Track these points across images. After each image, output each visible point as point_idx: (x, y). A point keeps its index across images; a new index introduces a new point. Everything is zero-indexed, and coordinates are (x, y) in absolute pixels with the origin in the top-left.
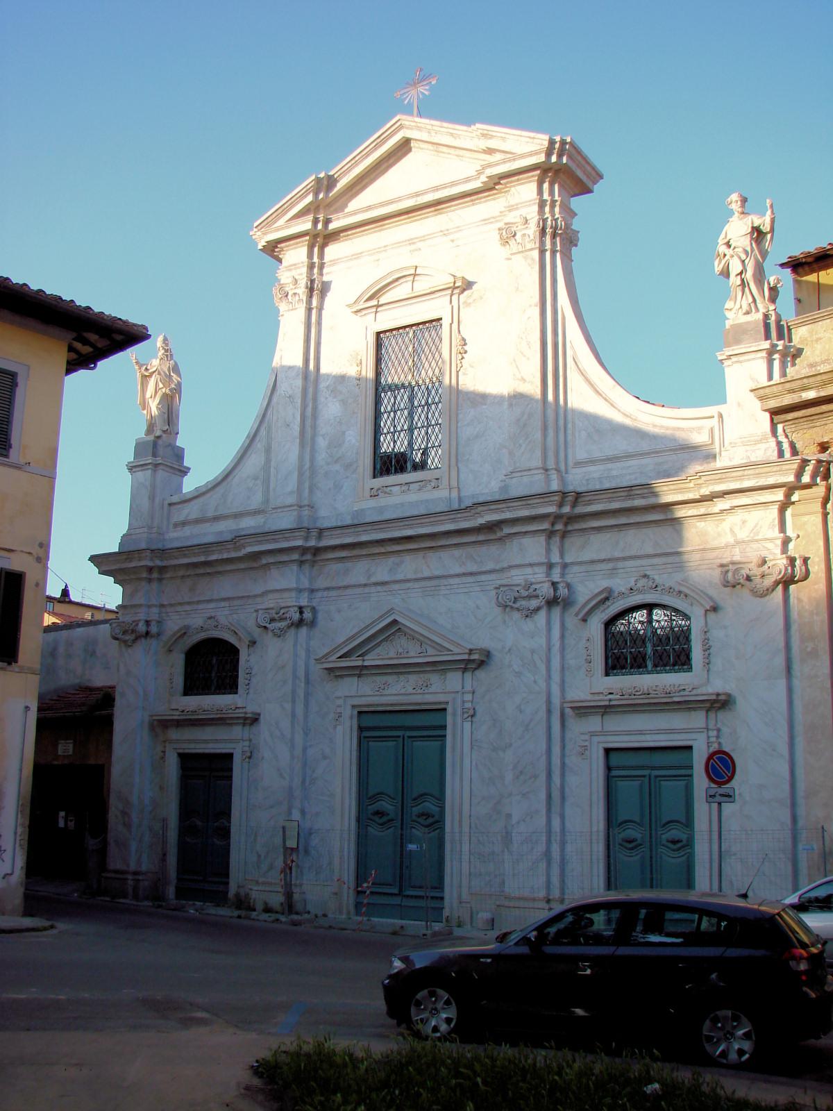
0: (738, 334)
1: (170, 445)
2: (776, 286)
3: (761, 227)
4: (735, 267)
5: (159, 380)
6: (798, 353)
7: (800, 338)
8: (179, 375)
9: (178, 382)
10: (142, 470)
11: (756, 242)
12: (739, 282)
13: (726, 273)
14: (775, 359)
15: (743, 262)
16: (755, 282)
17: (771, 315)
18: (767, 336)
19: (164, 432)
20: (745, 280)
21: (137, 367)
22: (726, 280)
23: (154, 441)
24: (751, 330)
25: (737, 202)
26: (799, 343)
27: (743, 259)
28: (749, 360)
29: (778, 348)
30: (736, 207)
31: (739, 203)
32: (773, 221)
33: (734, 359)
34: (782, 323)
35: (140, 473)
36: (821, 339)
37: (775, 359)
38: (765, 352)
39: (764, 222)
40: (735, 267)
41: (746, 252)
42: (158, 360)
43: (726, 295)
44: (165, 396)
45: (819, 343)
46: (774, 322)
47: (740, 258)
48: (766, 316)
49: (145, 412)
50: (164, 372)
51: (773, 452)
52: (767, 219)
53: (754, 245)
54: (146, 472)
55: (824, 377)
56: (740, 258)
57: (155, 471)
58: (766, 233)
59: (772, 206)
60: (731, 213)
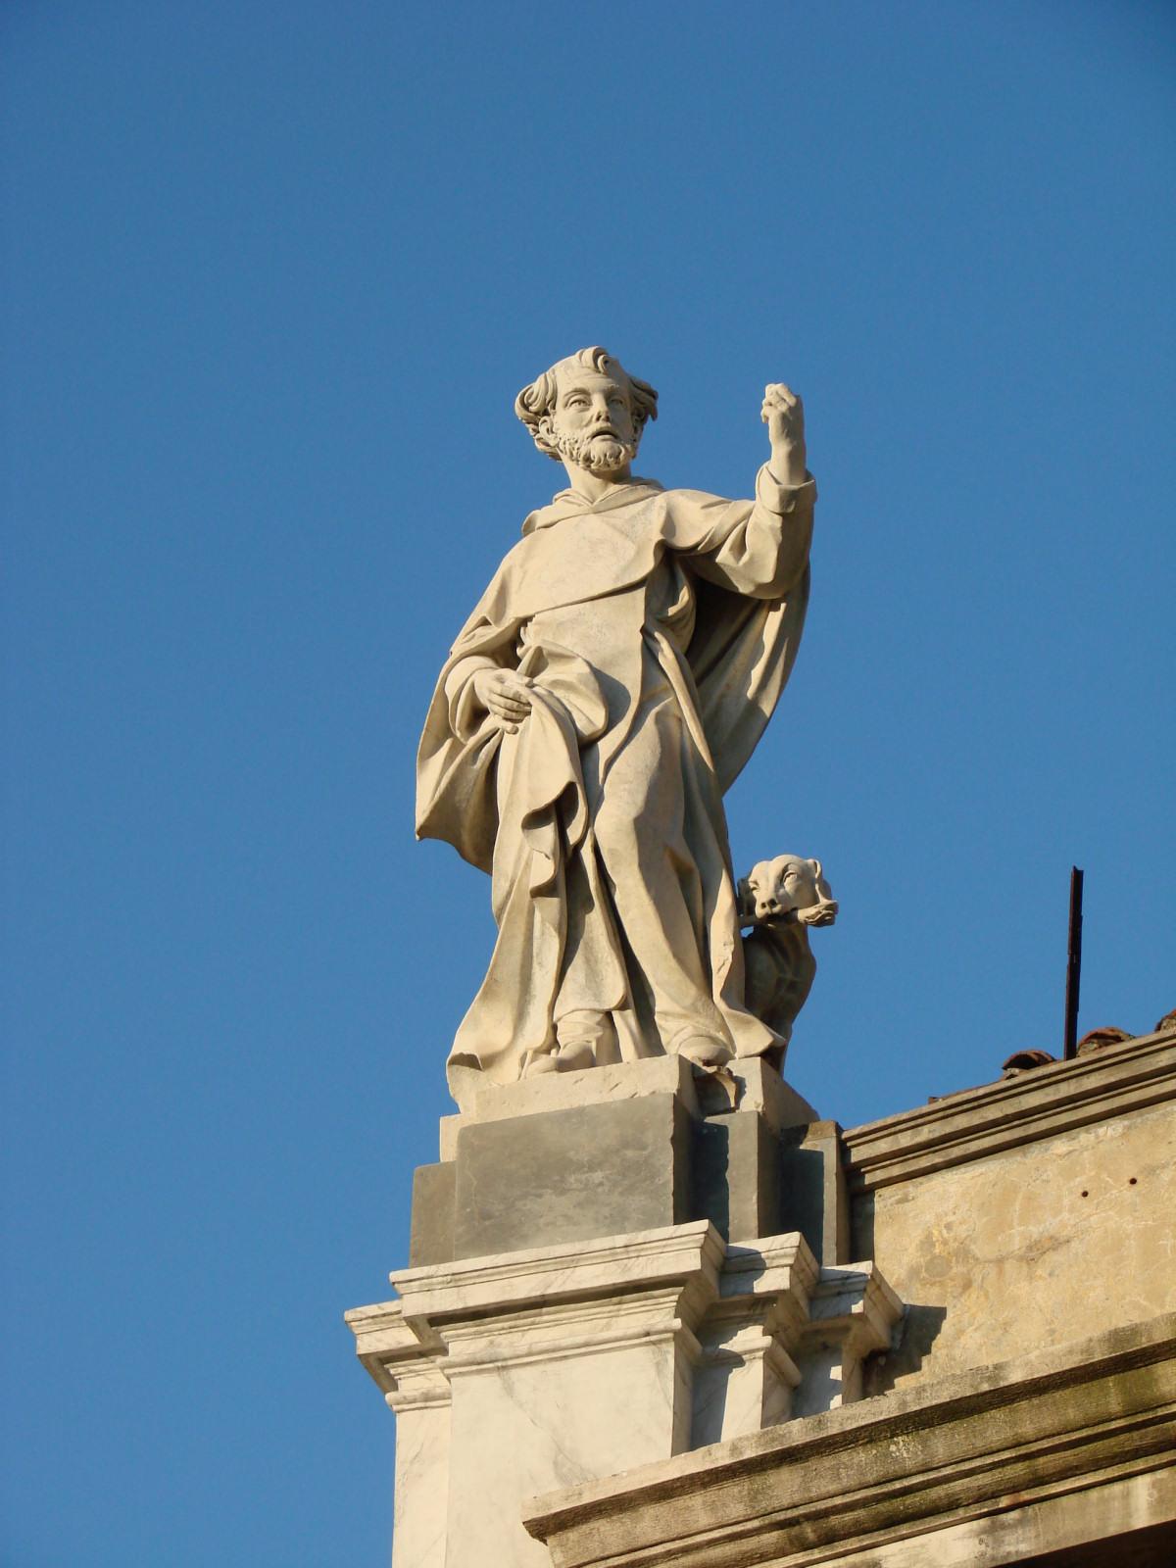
0: (520, 1181)
2: (788, 916)
3: (724, 557)
4: (535, 767)
6: (912, 1333)
7: (928, 1242)
11: (689, 656)
12: (544, 870)
13: (468, 827)
14: (737, 1360)
15: (583, 748)
16: (647, 868)
17: (740, 1084)
18: (698, 1190)
20: (587, 855)
22: (479, 872)
24: (592, 1167)
25: (583, 398)
26: (914, 1272)
27: (584, 727)
28: (557, 1354)
29: (763, 1285)
30: (574, 430)
31: (598, 405)
32: (797, 515)
33: (462, 1343)
34: (806, 1145)
36: (1056, 1243)
37: (737, 1360)
38: (670, 1299)
39: (746, 530)
40: (535, 767)
41: (611, 695)
43: (461, 966)
45: (1041, 1271)
46: (753, 1123)
47: (564, 720)
48: (704, 1088)
52: (762, 513)
53: (667, 657)
55: (1030, 1420)
56: (564, 720)
58: (753, 607)
59: (793, 424)
60: (548, 477)
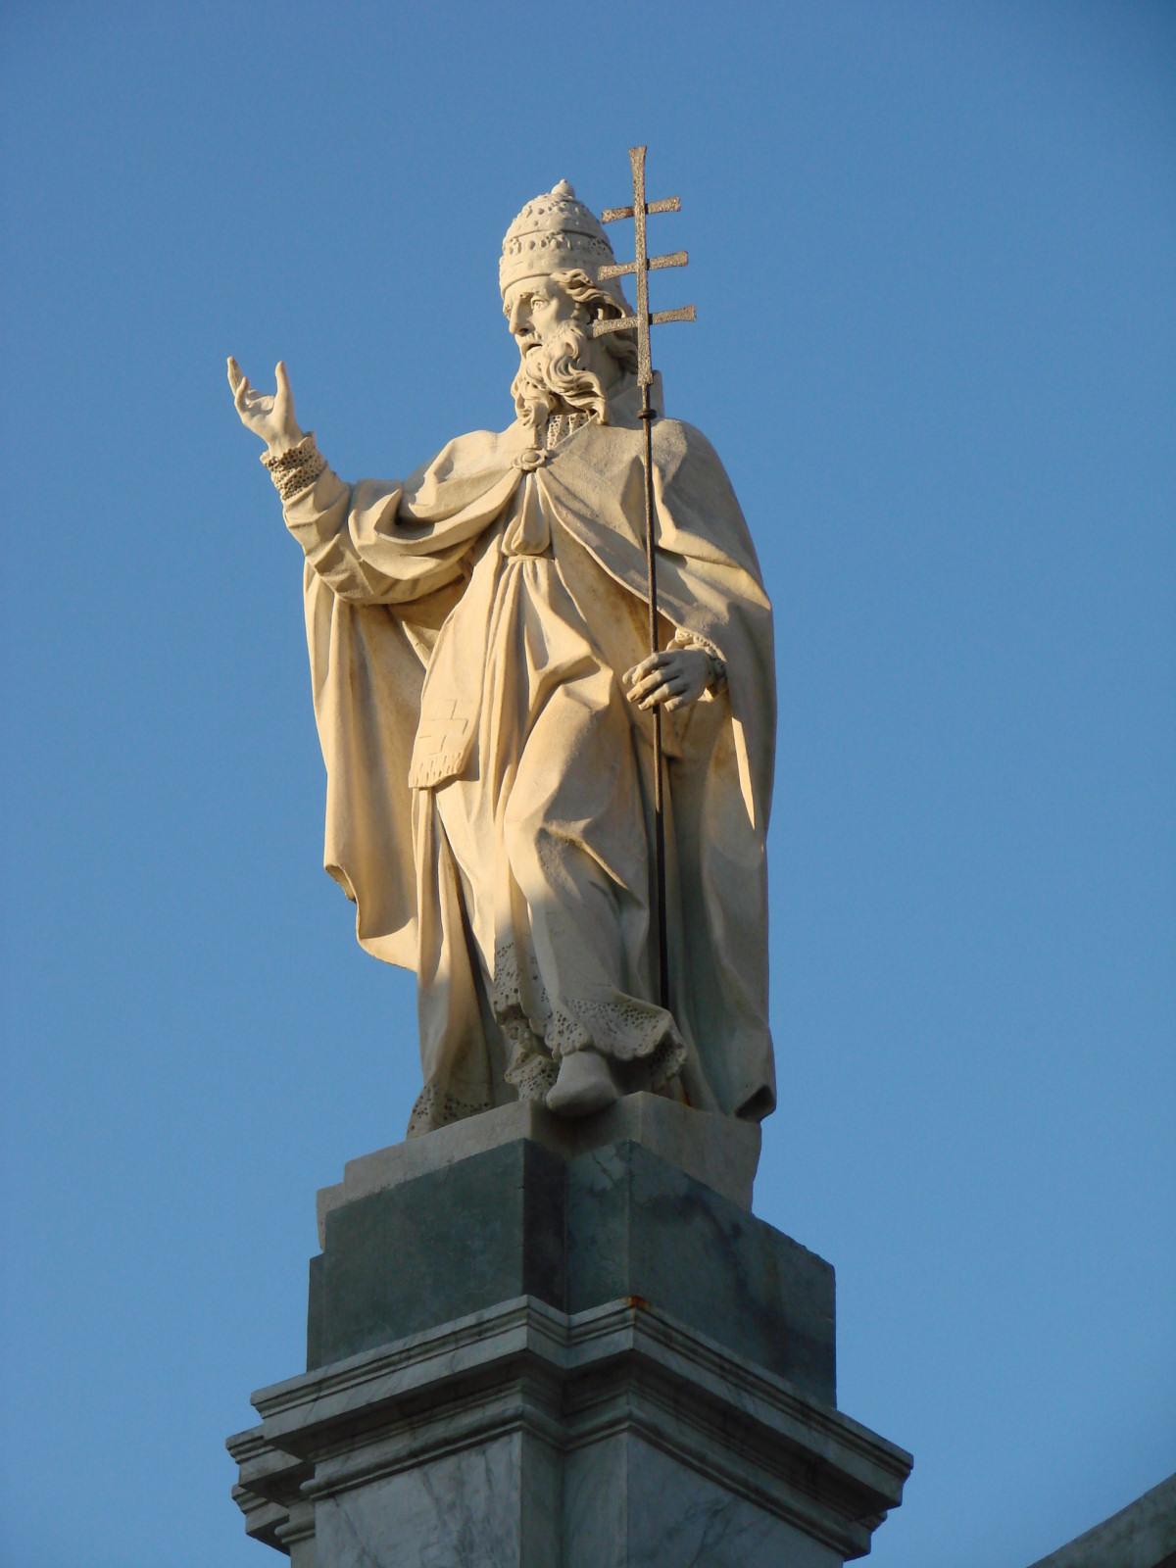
1: (694, 1202)
5: (538, 601)
8: (741, 549)
9: (738, 608)
10: (417, 1460)
19: (630, 1072)
21: (299, 515)
23: (529, 1146)
35: (403, 1488)
42: (520, 435)
44: (613, 735)
49: (402, 947)
50: (593, 522)
51: (504, 271)
54: (474, 1463)
57: (560, 1447)
